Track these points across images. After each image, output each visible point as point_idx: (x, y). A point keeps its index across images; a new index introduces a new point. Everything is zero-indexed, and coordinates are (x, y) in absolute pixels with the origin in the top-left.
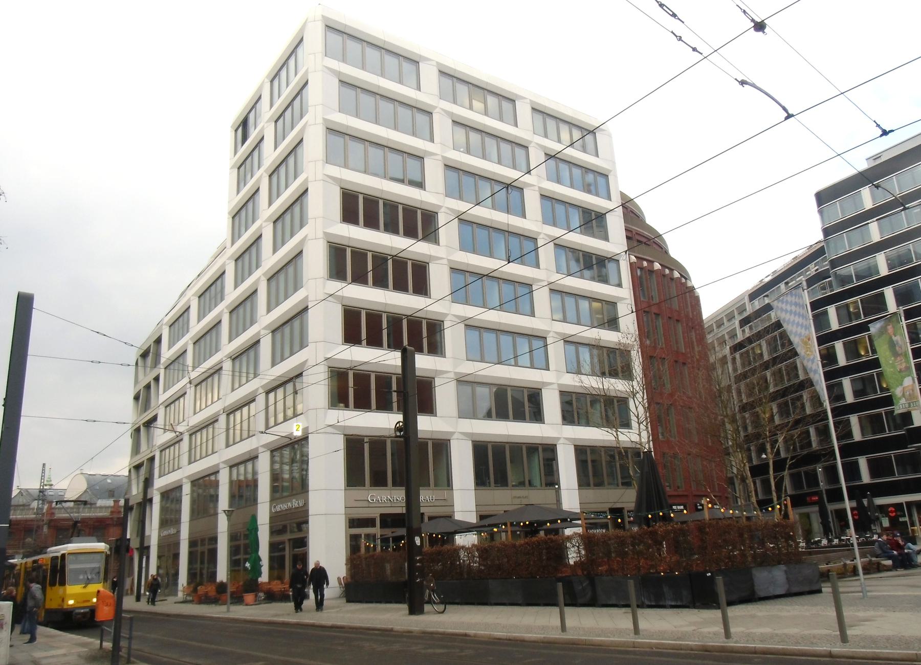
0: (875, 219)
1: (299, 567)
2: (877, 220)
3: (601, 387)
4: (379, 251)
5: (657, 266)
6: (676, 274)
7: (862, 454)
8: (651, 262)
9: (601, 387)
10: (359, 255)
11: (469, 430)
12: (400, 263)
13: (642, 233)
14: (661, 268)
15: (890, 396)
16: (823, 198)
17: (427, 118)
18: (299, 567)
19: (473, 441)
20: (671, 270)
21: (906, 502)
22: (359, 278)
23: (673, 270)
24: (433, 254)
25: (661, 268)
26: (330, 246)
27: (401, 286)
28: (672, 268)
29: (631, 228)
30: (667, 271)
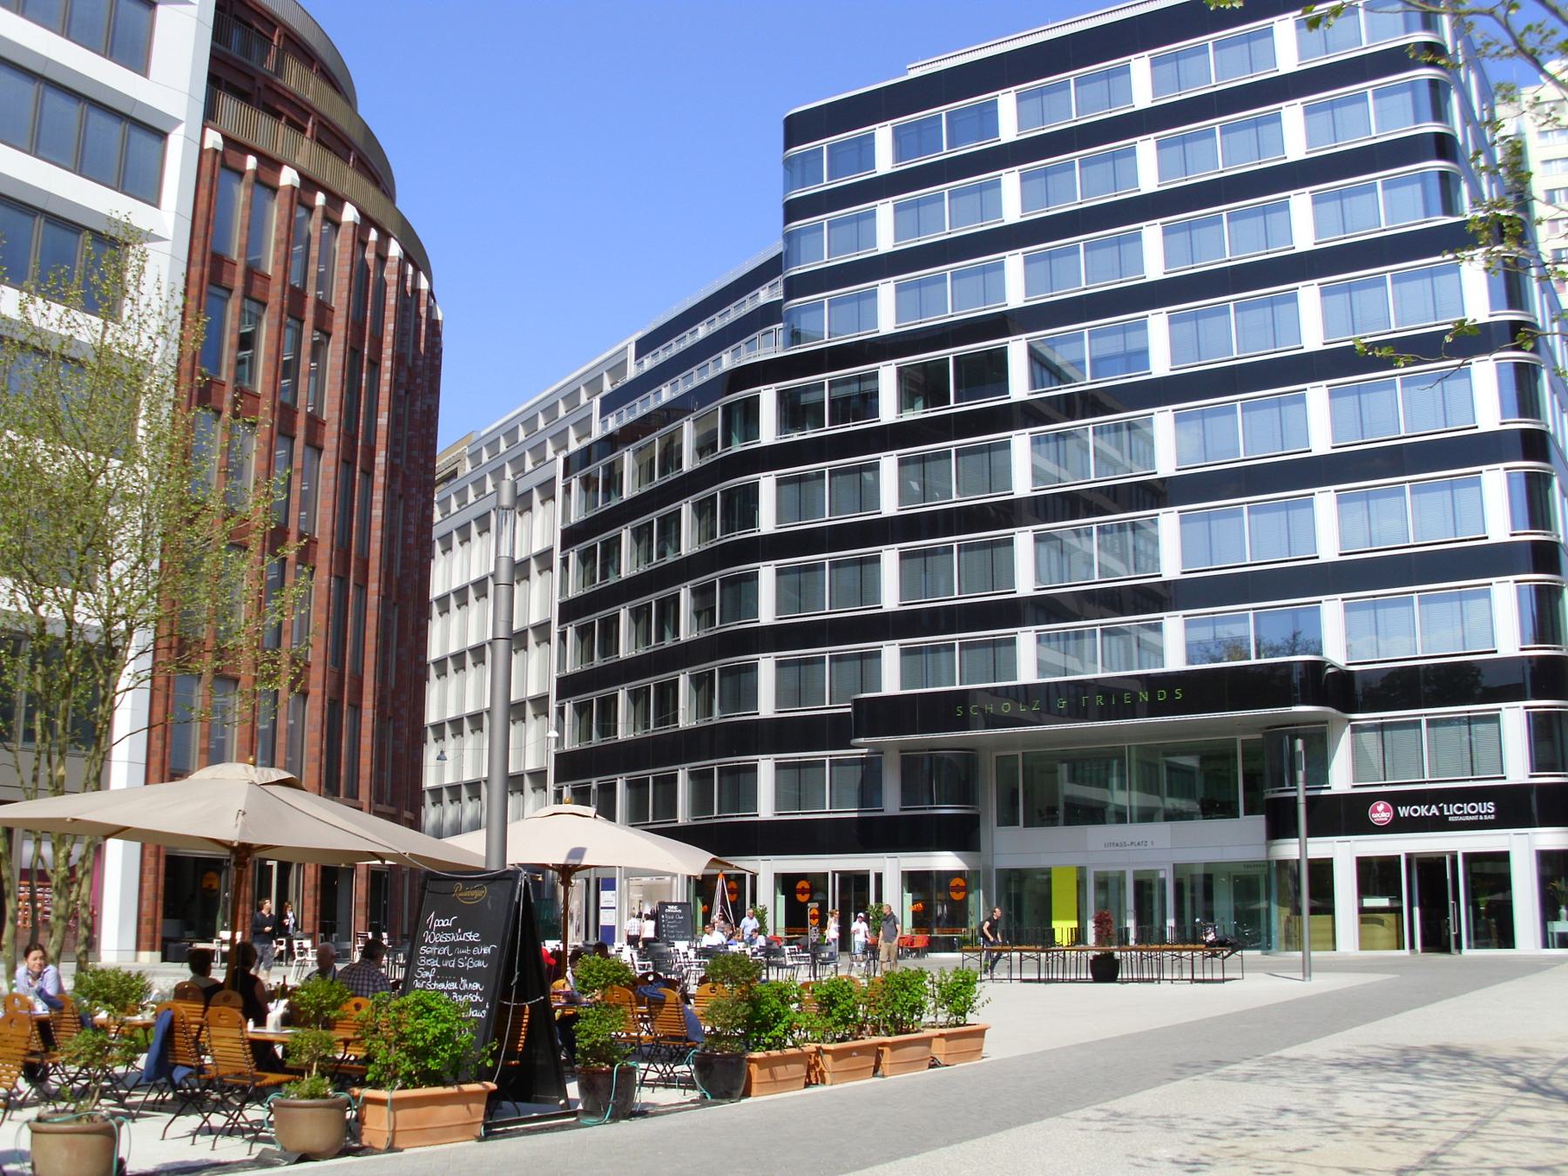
7: (1023, 405)
15: (260, 260)
16: (799, 128)
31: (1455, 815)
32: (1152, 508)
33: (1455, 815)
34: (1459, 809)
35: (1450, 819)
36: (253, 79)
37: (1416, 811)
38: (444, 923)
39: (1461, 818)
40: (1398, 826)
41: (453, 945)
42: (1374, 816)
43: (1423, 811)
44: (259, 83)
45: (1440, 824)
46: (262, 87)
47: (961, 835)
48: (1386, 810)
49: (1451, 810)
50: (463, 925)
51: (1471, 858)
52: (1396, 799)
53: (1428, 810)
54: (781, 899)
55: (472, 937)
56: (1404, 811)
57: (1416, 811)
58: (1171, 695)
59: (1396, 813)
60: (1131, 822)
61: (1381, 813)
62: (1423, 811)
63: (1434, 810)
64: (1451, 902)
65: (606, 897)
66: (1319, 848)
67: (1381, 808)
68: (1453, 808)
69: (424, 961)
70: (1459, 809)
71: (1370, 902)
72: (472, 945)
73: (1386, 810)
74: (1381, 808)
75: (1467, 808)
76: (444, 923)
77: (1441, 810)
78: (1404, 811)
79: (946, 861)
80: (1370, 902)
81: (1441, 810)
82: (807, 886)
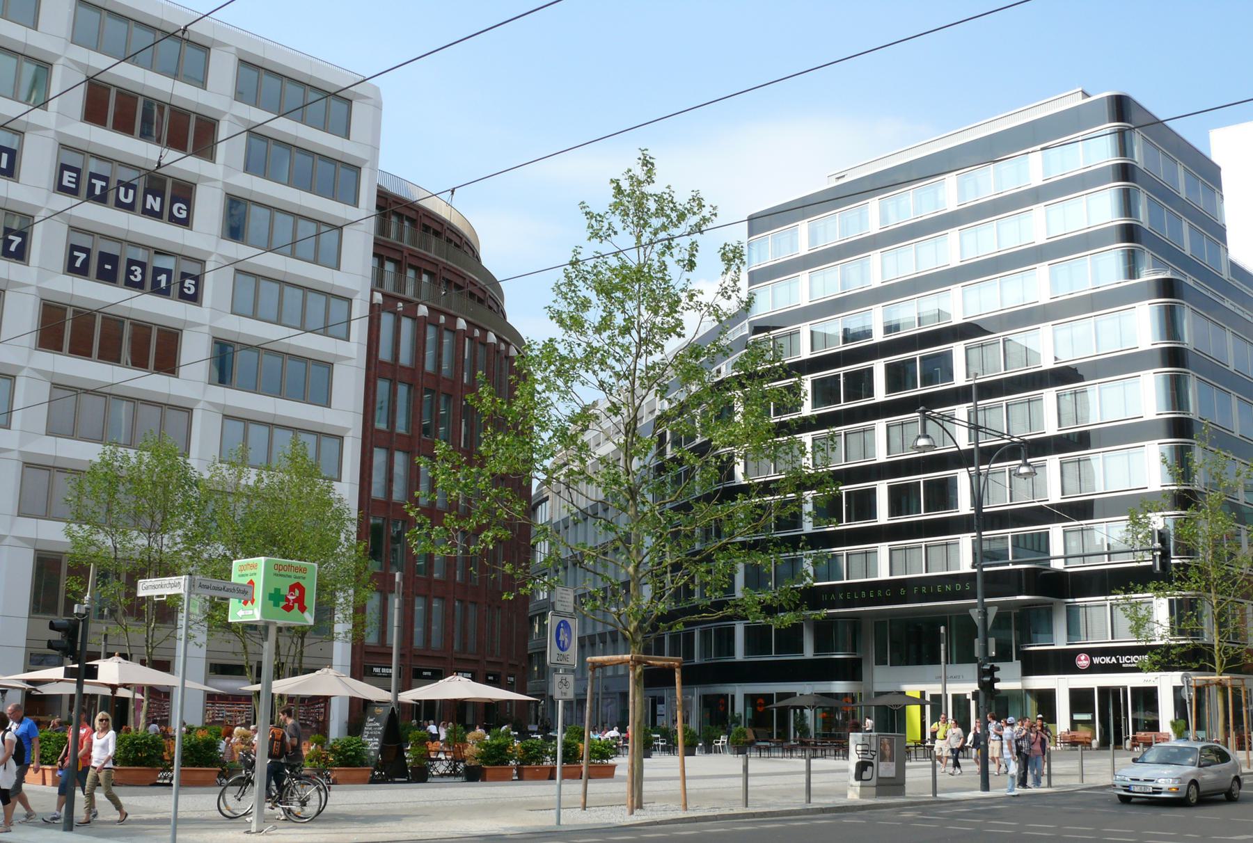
0: (1039, 147)
1: (326, 598)
2: (1042, 149)
3: (575, 510)
4: (141, 319)
5: (492, 338)
6: (513, 352)
8: (485, 331)
9: (575, 510)
10: (84, 318)
11: (31, 534)
12: (142, 330)
13: (460, 271)
14: (427, 315)
17: (354, 174)
18: (326, 598)
19: (36, 550)
20: (508, 344)
21: (777, 693)
22: (81, 349)
23: (487, 331)
24: (13, 278)
25: (427, 315)
26: (44, 304)
27: (139, 362)
28: (488, 328)
29: (465, 274)
30: (503, 346)
31: (1126, 663)
32: (1061, 435)
33: (1126, 663)
34: (1128, 659)
35: (1124, 665)
36: (402, 252)
37: (1103, 660)
38: (372, 720)
39: (1130, 665)
40: (1093, 669)
41: (373, 727)
42: (1079, 663)
43: (1107, 660)
44: (406, 253)
45: (1117, 668)
46: (408, 256)
47: (851, 671)
48: (1086, 659)
49: (1124, 660)
50: (376, 721)
51: (1135, 690)
52: (1092, 653)
53: (1110, 660)
54: (749, 709)
55: (378, 724)
56: (1096, 660)
57: (1103, 660)
58: (875, 594)
59: (1092, 661)
60: (951, 663)
61: (1083, 661)
62: (1107, 660)
63: (1114, 660)
64: (1123, 717)
65: (660, 707)
66: (1039, 682)
67: (1083, 658)
68: (1125, 659)
69: (365, 732)
70: (1128, 659)
71: (1077, 717)
72: (377, 727)
73: (1086, 659)
74: (1083, 658)
75: (1133, 659)
76: (372, 720)
77: (1117, 660)
78: (1096, 660)
79: (839, 687)
80: (1077, 717)
81: (1117, 660)
82: (763, 702)
